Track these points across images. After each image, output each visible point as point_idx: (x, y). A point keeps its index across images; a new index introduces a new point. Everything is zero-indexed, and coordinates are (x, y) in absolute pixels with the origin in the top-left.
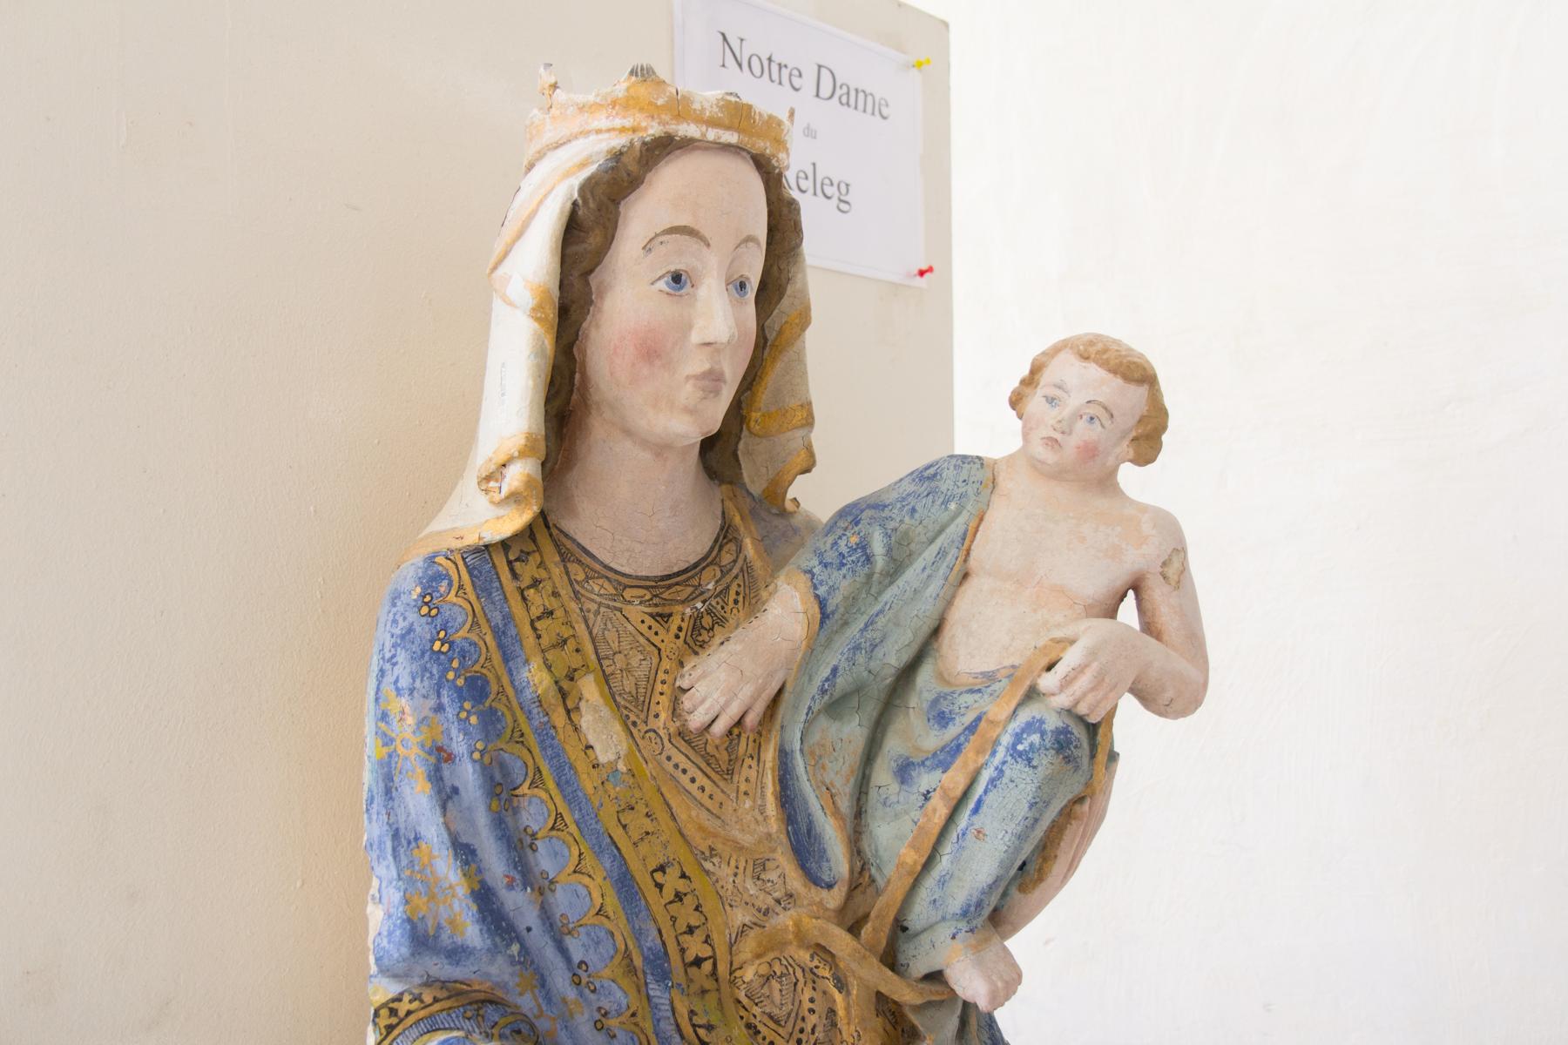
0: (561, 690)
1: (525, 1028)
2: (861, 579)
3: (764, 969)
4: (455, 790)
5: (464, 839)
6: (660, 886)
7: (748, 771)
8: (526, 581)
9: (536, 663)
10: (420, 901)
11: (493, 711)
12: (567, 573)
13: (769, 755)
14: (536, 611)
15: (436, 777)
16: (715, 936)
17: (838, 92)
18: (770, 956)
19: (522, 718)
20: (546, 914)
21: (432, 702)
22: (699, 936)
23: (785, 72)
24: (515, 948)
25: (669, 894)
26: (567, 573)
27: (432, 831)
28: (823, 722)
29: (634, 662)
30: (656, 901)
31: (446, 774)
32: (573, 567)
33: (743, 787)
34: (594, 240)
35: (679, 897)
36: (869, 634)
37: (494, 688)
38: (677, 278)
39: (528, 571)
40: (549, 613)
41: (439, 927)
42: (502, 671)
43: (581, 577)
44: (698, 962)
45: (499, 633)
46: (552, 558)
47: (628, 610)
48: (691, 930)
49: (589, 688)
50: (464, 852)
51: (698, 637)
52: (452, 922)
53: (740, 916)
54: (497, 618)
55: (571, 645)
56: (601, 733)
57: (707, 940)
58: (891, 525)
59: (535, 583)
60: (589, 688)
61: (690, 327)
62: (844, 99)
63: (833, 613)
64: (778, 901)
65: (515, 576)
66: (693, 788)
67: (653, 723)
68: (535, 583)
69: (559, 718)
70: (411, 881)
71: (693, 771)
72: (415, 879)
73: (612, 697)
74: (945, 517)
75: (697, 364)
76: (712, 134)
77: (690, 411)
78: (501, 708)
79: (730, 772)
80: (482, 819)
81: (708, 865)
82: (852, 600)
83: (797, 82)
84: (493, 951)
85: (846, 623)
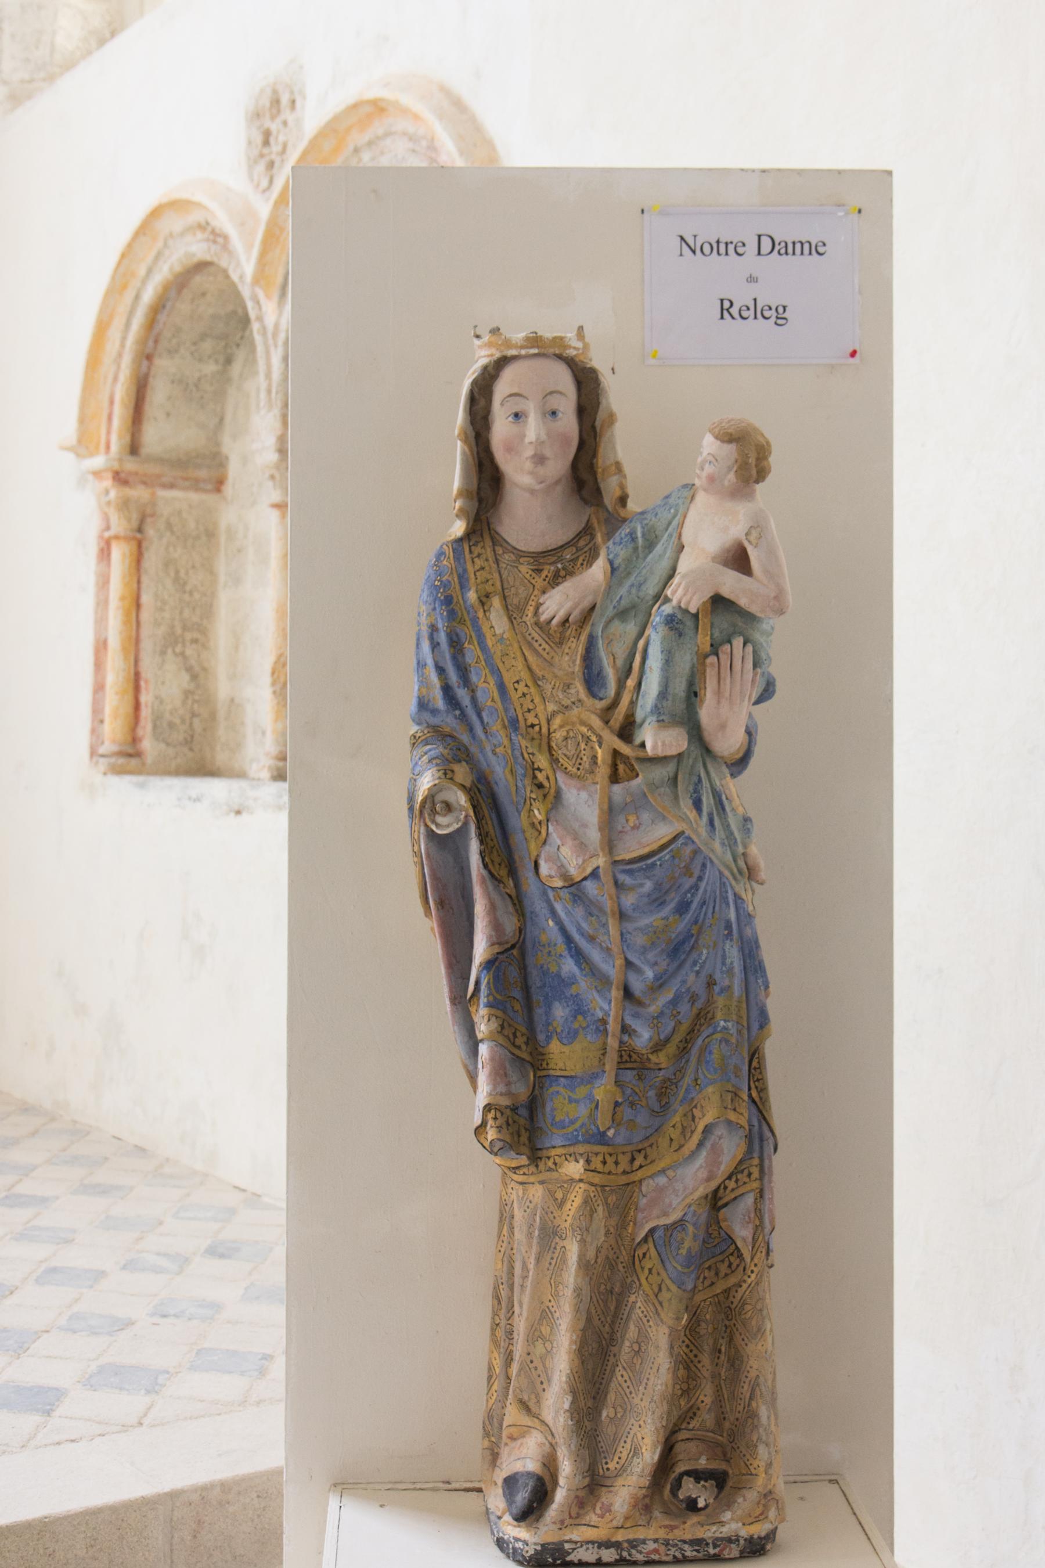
0: (481, 601)
1: (463, 749)
2: (630, 550)
3: (565, 734)
4: (438, 644)
5: (440, 665)
6: (516, 690)
7: (572, 643)
8: (476, 554)
9: (473, 589)
10: (424, 691)
11: (453, 610)
12: (494, 551)
13: (584, 638)
14: (477, 567)
15: (431, 638)
16: (540, 715)
17: (777, 248)
18: (568, 728)
19: (465, 614)
20: (474, 700)
21: (432, 606)
22: (533, 713)
23: (731, 248)
24: (458, 712)
25: (520, 693)
26: (494, 551)
27: (430, 662)
28: (616, 623)
29: (520, 591)
30: (515, 696)
31: (435, 637)
32: (497, 548)
33: (567, 651)
34: (482, 403)
35: (524, 695)
36: (638, 579)
37: (455, 600)
38: (516, 415)
39: (477, 550)
40: (483, 568)
41: (429, 701)
42: (459, 593)
43: (501, 552)
44: (533, 726)
45: (460, 577)
46: (488, 542)
47: (521, 568)
48: (529, 711)
49: (496, 602)
50: (441, 670)
51: (556, 580)
52: (434, 698)
53: (551, 707)
54: (460, 570)
55: (490, 583)
56: (497, 621)
57: (536, 716)
58: (646, 522)
59: (479, 556)
60: (496, 602)
61: (525, 436)
62: (783, 251)
63: (618, 567)
64: (574, 703)
65: (471, 552)
66: (540, 649)
67: (525, 619)
68: (479, 556)
69: (481, 614)
70: (422, 682)
71: (541, 641)
72: (424, 682)
73: (506, 607)
74: (670, 516)
75: (529, 452)
76: (523, 352)
77: (531, 473)
78: (457, 608)
79: (561, 643)
80: (448, 656)
81: (540, 683)
82: (628, 561)
83: (740, 250)
84: (448, 712)
85: (629, 574)
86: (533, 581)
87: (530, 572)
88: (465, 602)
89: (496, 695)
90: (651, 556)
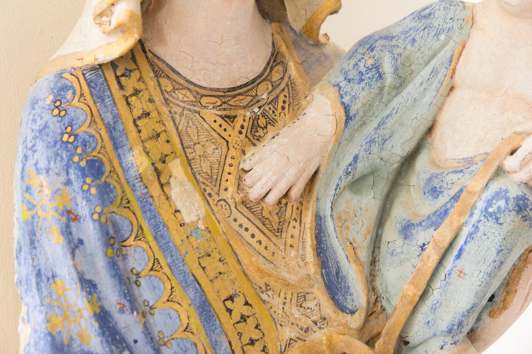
0: (156, 169)
5: (88, 277)
6: (230, 311)
7: (293, 230)
9: (138, 150)
11: (107, 185)
13: (308, 219)
14: (137, 113)
15: (67, 232)
19: (128, 190)
21: (63, 178)
25: (236, 316)
28: (348, 195)
29: (209, 151)
31: (74, 229)
33: (289, 241)
36: (381, 132)
37: (107, 168)
41: (71, 339)
42: (112, 155)
43: (169, 88)
45: (110, 129)
47: (205, 113)
48: (252, 342)
49: (176, 168)
50: (89, 286)
51: (255, 132)
54: (109, 117)
55: (163, 137)
56: (185, 200)
58: (397, 51)
59: (136, 93)
64: (315, 323)
67: (223, 195)
68: (136, 93)
69: (155, 190)
70: (50, 306)
71: (253, 230)
72: (53, 305)
78: (113, 182)
81: (264, 296)
82: (369, 106)
86: (225, 135)
87: (220, 121)
88: (125, 171)
89: (196, 323)
90: (398, 100)
